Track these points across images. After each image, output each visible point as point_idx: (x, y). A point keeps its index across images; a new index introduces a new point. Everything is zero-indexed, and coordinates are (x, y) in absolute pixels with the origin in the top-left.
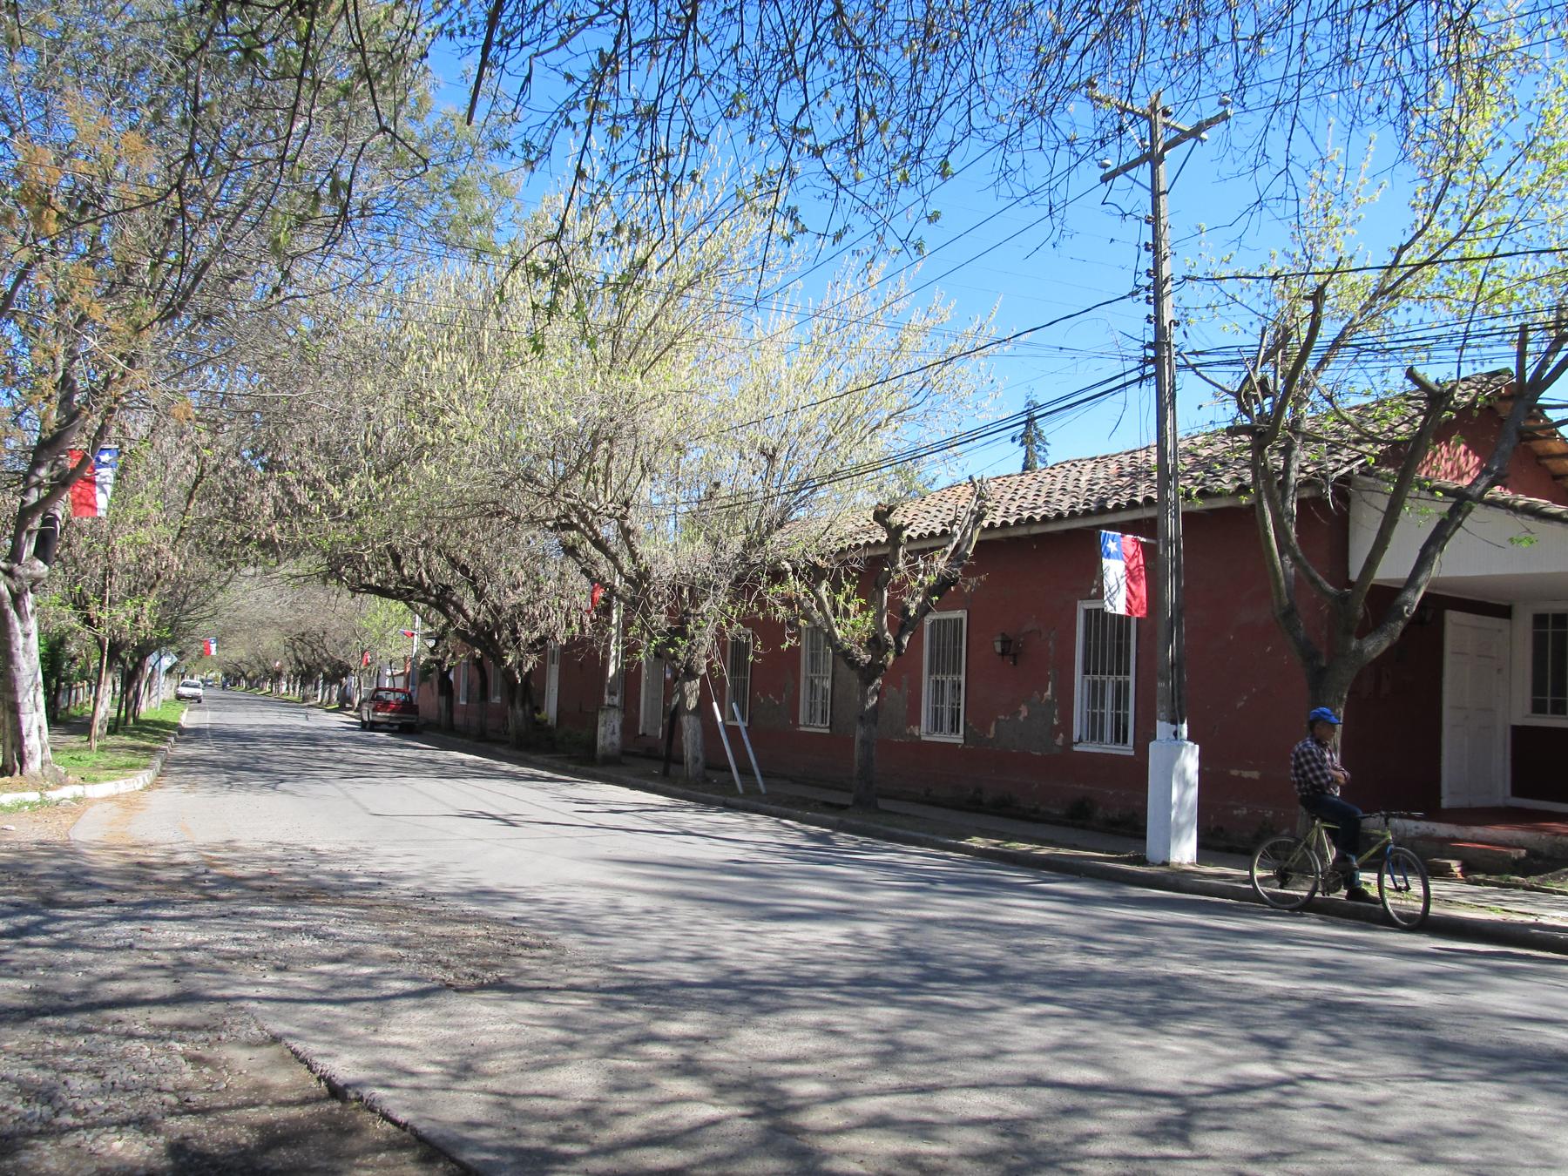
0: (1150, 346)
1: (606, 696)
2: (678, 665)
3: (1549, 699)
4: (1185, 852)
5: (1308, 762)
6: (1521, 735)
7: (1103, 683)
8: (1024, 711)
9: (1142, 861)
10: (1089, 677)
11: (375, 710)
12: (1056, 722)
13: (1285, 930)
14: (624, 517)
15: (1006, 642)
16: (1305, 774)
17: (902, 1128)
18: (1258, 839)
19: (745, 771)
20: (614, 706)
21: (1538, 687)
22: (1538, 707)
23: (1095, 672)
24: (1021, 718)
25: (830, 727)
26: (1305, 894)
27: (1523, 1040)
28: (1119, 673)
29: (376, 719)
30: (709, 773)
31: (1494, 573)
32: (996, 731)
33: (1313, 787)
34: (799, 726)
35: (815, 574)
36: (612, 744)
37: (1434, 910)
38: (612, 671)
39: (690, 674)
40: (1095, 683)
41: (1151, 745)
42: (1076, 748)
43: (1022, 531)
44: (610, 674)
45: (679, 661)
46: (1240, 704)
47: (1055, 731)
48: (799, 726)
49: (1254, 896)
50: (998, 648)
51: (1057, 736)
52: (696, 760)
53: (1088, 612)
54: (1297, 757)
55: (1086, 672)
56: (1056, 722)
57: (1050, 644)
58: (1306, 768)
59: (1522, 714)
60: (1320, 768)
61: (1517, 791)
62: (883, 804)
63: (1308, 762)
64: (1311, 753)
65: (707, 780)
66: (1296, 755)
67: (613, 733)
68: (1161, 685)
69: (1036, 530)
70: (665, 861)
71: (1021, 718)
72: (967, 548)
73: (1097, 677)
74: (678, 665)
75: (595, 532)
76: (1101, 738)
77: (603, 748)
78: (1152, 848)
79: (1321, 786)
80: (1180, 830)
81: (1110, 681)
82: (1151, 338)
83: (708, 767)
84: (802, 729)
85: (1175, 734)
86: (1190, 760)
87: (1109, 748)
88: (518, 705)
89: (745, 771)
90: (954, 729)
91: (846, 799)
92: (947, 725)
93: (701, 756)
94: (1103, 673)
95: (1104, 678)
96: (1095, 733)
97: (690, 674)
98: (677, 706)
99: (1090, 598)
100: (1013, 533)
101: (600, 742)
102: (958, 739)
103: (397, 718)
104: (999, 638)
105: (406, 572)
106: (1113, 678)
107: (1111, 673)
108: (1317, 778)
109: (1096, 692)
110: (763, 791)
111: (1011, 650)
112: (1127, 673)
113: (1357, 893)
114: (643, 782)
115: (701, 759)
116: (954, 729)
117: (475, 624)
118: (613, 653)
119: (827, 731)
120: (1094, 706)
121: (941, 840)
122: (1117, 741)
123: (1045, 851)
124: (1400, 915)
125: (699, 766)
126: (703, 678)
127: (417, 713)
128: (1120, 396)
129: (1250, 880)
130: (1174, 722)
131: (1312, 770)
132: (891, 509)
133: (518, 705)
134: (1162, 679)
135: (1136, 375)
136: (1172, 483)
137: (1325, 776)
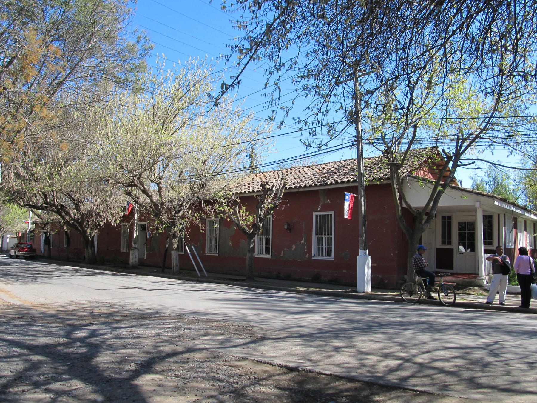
0: (355, 136)
1: (133, 244)
2: (171, 233)
3: (446, 240)
4: (368, 289)
5: (418, 261)
6: (439, 251)
7: (322, 238)
8: (294, 247)
9: (356, 292)
10: (317, 236)
11: (19, 251)
12: (306, 250)
13: (429, 306)
14: (160, 183)
15: (288, 225)
16: (417, 264)
17: (400, 358)
18: (402, 284)
19: (200, 270)
20: (136, 248)
21: (443, 237)
22: (443, 243)
23: (320, 234)
24: (293, 249)
25: (218, 254)
26: (418, 298)
27: (515, 329)
28: (328, 235)
29: (19, 254)
30: (181, 271)
31: (445, 205)
32: (284, 254)
33: (420, 268)
34: (205, 253)
35: (232, 204)
36: (135, 261)
37: (457, 301)
38: (135, 236)
39: (175, 236)
40: (319, 238)
41: (358, 257)
42: (313, 258)
43: (296, 190)
44: (134, 237)
45: (171, 232)
46: (370, 244)
47: (306, 253)
48: (205, 253)
49: (402, 300)
50: (286, 227)
51: (306, 254)
52: (177, 266)
53: (317, 216)
54: (415, 259)
55: (316, 234)
56: (306, 250)
57: (303, 226)
58: (418, 262)
59: (439, 245)
60: (422, 262)
61: (437, 267)
62: (256, 279)
63: (418, 261)
64: (419, 258)
65: (181, 273)
66: (415, 259)
67: (136, 257)
68: (360, 239)
69: (301, 190)
70: (222, 299)
71: (293, 249)
72: (280, 195)
73: (320, 236)
74: (171, 233)
75: (144, 188)
76: (322, 255)
77: (132, 263)
78: (359, 288)
79: (422, 267)
80: (367, 283)
81: (325, 237)
82: (355, 134)
83: (180, 269)
84: (206, 254)
85: (365, 253)
86: (369, 260)
87: (324, 258)
88: (89, 248)
89: (200, 270)
90: (267, 252)
91: (244, 278)
92: (264, 252)
93: (178, 265)
94: (322, 234)
95: (323, 236)
96: (320, 253)
97: (175, 236)
98: (167, 248)
99: (317, 211)
100: (292, 191)
101: (131, 261)
102: (269, 256)
103: (27, 254)
104: (286, 224)
105: (48, 200)
106: (326, 236)
107: (325, 235)
108: (421, 265)
109: (320, 241)
110: (207, 276)
111: (290, 228)
112: (331, 234)
113: (432, 298)
114: (152, 274)
115: (178, 266)
116: (267, 252)
117: (73, 219)
118: (135, 230)
119: (217, 255)
120: (319, 245)
121: (290, 289)
122: (267, 254)
123: (325, 290)
124: (445, 302)
125: (178, 268)
126: (179, 238)
127: (35, 252)
128: (341, 151)
129: (400, 295)
130: (365, 250)
131: (420, 263)
132: (267, 183)
133: (89, 248)
134: (361, 237)
135: (351, 144)
136: (363, 178)
137: (423, 264)
